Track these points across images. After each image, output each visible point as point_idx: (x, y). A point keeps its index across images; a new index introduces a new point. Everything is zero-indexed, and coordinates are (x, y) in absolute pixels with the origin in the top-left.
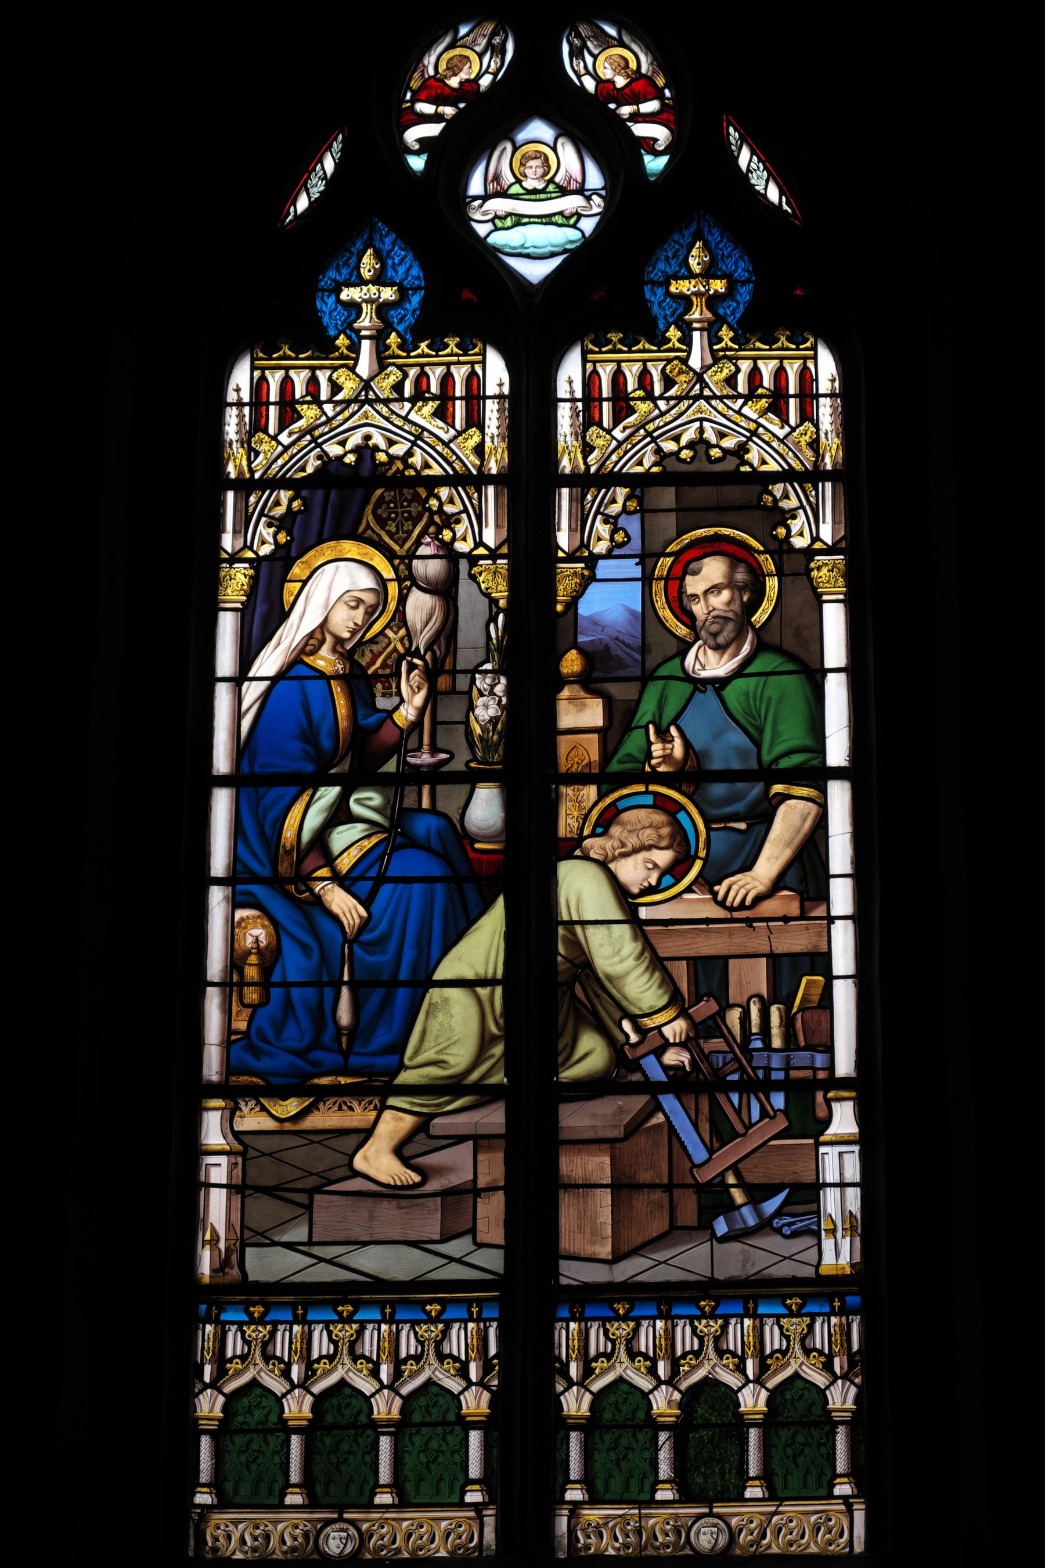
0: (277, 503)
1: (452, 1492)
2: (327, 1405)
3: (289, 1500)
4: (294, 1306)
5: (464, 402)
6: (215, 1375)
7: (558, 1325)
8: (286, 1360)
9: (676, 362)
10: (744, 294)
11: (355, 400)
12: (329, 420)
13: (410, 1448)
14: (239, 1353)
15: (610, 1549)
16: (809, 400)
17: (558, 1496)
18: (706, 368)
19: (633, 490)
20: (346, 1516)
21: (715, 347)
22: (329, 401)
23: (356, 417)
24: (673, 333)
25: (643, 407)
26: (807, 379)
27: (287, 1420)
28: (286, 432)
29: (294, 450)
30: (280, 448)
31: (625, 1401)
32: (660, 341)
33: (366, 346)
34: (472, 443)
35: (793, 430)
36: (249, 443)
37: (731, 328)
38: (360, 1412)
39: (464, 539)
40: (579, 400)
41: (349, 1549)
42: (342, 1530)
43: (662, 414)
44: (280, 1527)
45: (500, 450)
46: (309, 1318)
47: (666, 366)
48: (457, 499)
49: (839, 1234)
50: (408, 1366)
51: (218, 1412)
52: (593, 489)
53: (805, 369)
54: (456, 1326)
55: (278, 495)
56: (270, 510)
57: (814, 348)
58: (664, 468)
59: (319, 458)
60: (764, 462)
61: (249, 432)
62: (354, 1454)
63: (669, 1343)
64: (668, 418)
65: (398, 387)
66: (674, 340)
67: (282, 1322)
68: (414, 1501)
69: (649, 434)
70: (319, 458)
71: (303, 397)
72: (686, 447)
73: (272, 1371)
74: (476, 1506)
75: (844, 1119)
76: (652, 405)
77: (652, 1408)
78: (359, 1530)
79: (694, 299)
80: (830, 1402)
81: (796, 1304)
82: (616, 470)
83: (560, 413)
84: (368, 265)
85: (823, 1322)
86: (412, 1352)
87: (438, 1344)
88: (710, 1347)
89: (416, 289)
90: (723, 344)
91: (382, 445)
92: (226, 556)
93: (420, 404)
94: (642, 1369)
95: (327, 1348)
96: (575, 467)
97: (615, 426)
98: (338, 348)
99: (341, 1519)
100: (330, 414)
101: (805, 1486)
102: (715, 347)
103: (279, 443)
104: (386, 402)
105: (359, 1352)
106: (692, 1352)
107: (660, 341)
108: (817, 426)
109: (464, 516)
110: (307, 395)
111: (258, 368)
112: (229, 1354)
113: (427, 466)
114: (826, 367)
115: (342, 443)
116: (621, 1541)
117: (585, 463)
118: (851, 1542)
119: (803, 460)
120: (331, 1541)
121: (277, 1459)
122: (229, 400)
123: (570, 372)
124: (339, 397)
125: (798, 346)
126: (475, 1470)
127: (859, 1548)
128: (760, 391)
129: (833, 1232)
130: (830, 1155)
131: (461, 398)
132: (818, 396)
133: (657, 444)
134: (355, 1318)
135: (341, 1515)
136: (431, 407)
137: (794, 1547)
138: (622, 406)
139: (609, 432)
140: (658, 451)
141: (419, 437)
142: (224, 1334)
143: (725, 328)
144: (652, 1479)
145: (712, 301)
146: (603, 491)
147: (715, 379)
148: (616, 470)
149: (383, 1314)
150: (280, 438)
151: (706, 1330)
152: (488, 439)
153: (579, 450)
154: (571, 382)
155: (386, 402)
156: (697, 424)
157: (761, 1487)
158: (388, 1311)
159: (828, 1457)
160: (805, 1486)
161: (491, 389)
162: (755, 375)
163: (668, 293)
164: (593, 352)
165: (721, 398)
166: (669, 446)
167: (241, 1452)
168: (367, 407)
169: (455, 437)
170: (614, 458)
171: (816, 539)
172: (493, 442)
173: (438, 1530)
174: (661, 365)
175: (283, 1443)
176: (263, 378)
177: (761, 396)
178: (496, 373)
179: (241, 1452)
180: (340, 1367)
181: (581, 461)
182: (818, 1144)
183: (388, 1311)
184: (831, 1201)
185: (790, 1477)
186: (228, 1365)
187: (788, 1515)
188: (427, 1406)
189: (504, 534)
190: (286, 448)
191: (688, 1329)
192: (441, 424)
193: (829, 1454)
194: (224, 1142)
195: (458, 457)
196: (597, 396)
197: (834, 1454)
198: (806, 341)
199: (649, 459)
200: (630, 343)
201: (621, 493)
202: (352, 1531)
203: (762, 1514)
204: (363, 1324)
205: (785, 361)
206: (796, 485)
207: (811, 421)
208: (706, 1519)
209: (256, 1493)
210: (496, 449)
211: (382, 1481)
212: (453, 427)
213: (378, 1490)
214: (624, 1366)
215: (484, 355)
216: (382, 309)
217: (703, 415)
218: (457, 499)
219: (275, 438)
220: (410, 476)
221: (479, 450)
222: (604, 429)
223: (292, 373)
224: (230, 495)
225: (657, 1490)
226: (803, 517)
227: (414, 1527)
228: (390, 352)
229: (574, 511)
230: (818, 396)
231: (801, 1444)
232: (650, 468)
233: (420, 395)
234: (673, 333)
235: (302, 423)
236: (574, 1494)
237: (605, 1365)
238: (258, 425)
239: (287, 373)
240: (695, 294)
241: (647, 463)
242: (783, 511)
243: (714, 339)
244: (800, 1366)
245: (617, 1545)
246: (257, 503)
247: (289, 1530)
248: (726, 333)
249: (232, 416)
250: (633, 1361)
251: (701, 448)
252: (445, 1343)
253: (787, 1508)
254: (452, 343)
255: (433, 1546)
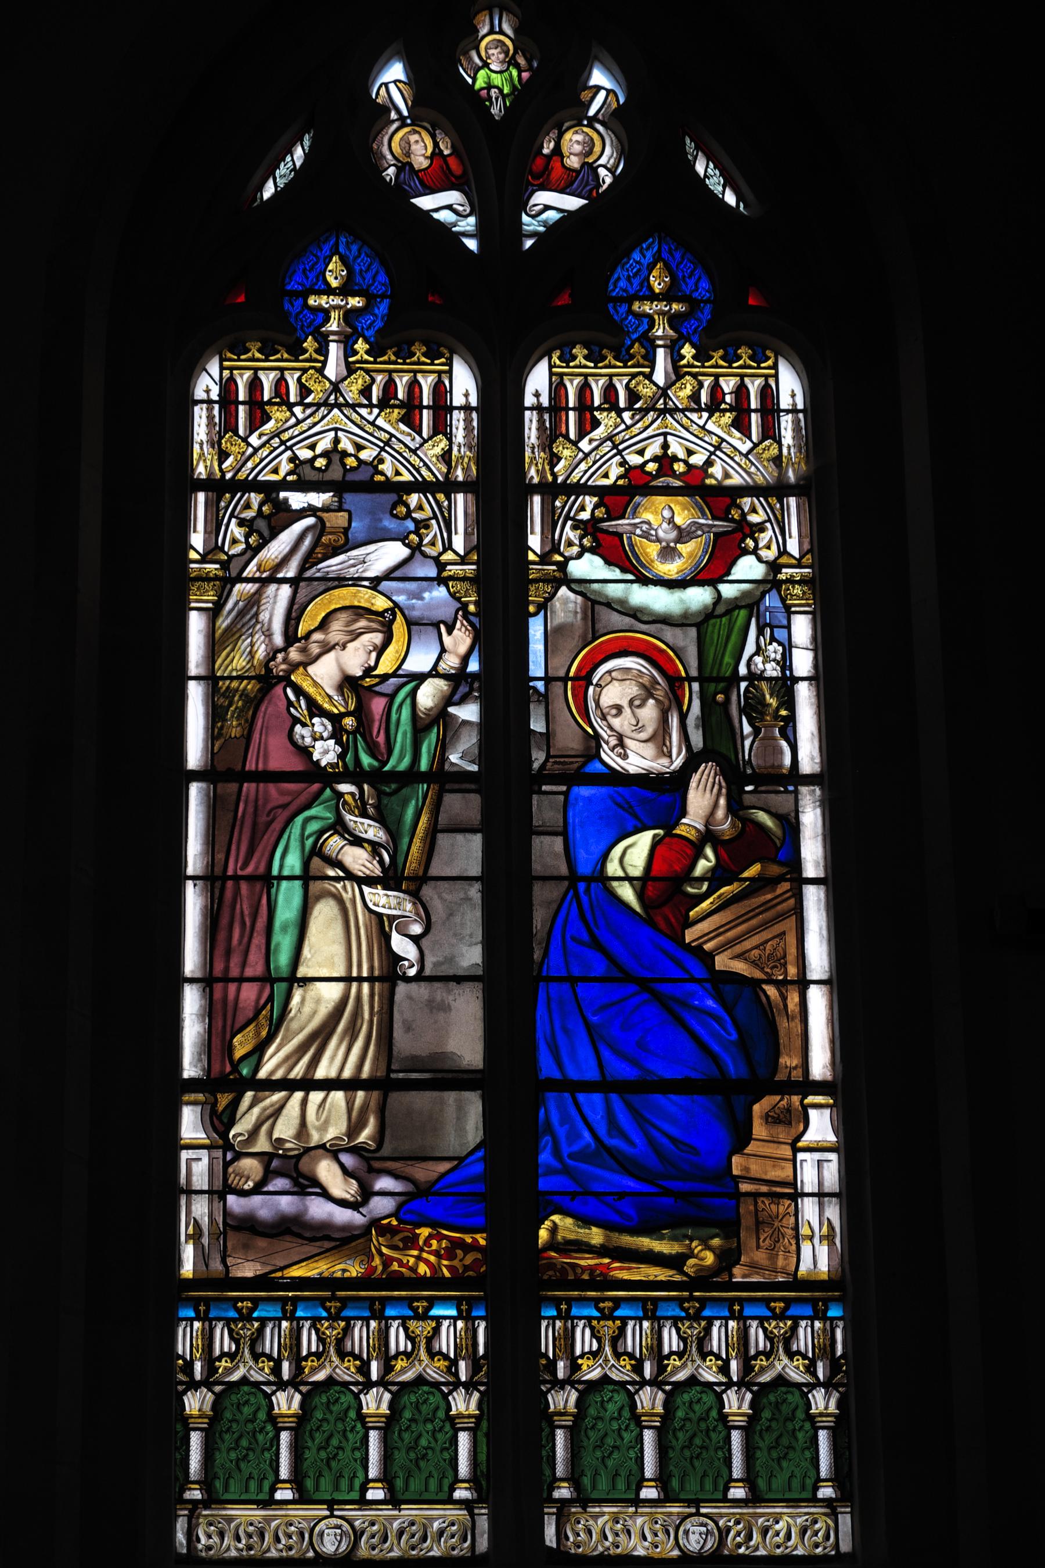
0: (248, 506)
1: (351, 1489)
2: (316, 1400)
3: (370, 1495)
4: (814, 1302)
5: (431, 412)
6: (294, 1372)
7: (544, 1324)
8: (724, 1356)
9: (311, 371)
10: (706, 313)
11: (325, 404)
12: (628, 428)
13: (310, 1444)
14: (587, 1349)
15: (639, 1548)
16: (442, 412)
17: (545, 1495)
18: (669, 385)
19: (601, 499)
20: (703, 1511)
21: (351, 359)
22: (629, 408)
23: (325, 421)
24: (309, 344)
25: (278, 414)
26: (768, 395)
27: (728, 1415)
28: (257, 433)
29: (264, 452)
30: (250, 450)
31: (425, 1401)
32: (296, 351)
33: (660, 353)
34: (438, 450)
35: (756, 445)
36: (220, 444)
37: (693, 346)
38: (437, 1408)
39: (768, 547)
40: (800, 411)
41: (343, 1547)
42: (702, 1525)
43: (299, 422)
44: (601, 1521)
45: (466, 460)
46: (658, 1314)
47: (630, 381)
48: (426, 506)
49: (816, 1240)
50: (223, 1363)
51: (384, 1409)
52: (227, 495)
53: (439, 384)
54: (270, 1325)
55: (249, 498)
56: (241, 512)
57: (775, 366)
58: (630, 481)
59: (621, 464)
60: (398, 473)
61: (219, 432)
62: (252, 1450)
63: (206, 1343)
64: (304, 426)
65: (366, 392)
66: (362, 352)
67: (803, 1318)
68: (766, 1497)
69: (283, 443)
70: (621, 464)
71: (271, 398)
72: (321, 455)
73: (710, 1368)
74: (828, 1502)
75: (821, 1126)
76: (288, 414)
77: (362, 1408)
78: (716, 1523)
79: (656, 317)
80: (727, 1406)
81: (247, 1307)
82: (582, 481)
83: (783, 425)
84: (334, 274)
85: (635, 1325)
86: (675, 1348)
87: (429, 1341)
88: (246, 1351)
89: (383, 296)
90: (358, 357)
91: (351, 450)
92: (197, 557)
93: (717, 414)
94: (267, 1370)
95: (228, 1345)
96: (210, 474)
97: (251, 433)
98: (305, 351)
99: (698, 1514)
100: (629, 422)
101: (702, 1489)
102: (351, 359)
103: (249, 444)
104: (353, 407)
105: (621, 1350)
106: (591, 1352)
107: (296, 351)
108: (450, 440)
109: (433, 522)
110: (275, 397)
111: (226, 369)
112: (304, 1353)
113: (727, 475)
114: (790, 386)
115: (312, 447)
116: (649, 1539)
117: (221, 470)
118: (837, 1545)
119: (763, 474)
120: (326, 1538)
121: (446, 1455)
122: (783, 406)
123: (538, 381)
124: (308, 400)
125: (759, 364)
126: (464, 1468)
127: (845, 1546)
128: (723, 406)
129: (811, 1238)
130: (808, 1163)
131: (428, 407)
132: (452, 408)
133: (623, 457)
134: (255, 1315)
135: (698, 1508)
136: (728, 418)
137: (377, 1551)
138: (259, 415)
139: (575, 443)
140: (294, 459)
141: (387, 443)
142: (299, 1330)
143: (360, 341)
144: (726, 1478)
145: (674, 320)
146: (573, 498)
147: (351, 391)
148: (582, 481)
149: (284, 1311)
150: (250, 440)
151: (689, 1332)
152: (455, 449)
153: (216, 457)
154: (793, 396)
155: (353, 407)
156: (332, 434)
157: (291, 1489)
158: (202, 1308)
159: (450, 1462)
160: (702, 1489)
161: (785, 403)
162: (390, 387)
163: (630, 311)
164: (555, 366)
165: (683, 411)
166: (305, 454)
167: (409, 1449)
168: (336, 411)
169: (422, 445)
170: (250, 465)
171: (783, 552)
172: (459, 451)
173: (786, 1528)
174: (297, 374)
175: (272, 1440)
176: (232, 379)
177: (725, 411)
178: (464, 384)
179: (409, 1449)
180: (241, 1365)
181: (216, 468)
182: (796, 1150)
183: (464, 1307)
184: (809, 1209)
185: (412, 1479)
186: (304, 1363)
187: (289, 1518)
188: (691, 1403)
189: (806, 546)
190: (587, 455)
191: (588, 1331)
192: (737, 434)
193: (182, 1459)
194: (204, 1136)
195: (425, 464)
196: (417, 403)
197: (456, 1459)
198: (767, 359)
199: (285, 467)
200: (268, 352)
201: (590, 501)
202: (346, 1526)
203: (305, 1518)
204: (796, 1320)
205: (286, 372)
206: (761, 499)
207: (445, 434)
208: (326, 1521)
209: (337, 1488)
210: (462, 458)
211: (735, 1476)
212: (750, 438)
213: (279, 1485)
214: (783, 1363)
215: (451, 365)
216: (350, 316)
217: (338, 426)
218: (426, 506)
219: (245, 440)
220: (380, 482)
221: (446, 457)
222: (240, 437)
223: (419, 377)
224: (537, 499)
225: (368, 1489)
226: (770, 532)
227: (406, 1524)
228: (684, 362)
229: (803, 522)
230: (452, 408)
231: (424, 1448)
232: (616, 481)
233: (714, 407)
234: (309, 344)
235: (270, 426)
236: (563, 1492)
237: (315, 1364)
238: (230, 425)
239: (256, 374)
240: (656, 312)
241: (282, 472)
242: (752, 525)
243: (349, 351)
244: (248, 1371)
245: (646, 1544)
246: (563, 507)
247: (283, 1527)
248: (361, 346)
249: (200, 415)
250: (257, 1362)
251: (336, 458)
252: (260, 1342)
253: (410, 1512)
254: (579, 352)
255: (425, 1545)
